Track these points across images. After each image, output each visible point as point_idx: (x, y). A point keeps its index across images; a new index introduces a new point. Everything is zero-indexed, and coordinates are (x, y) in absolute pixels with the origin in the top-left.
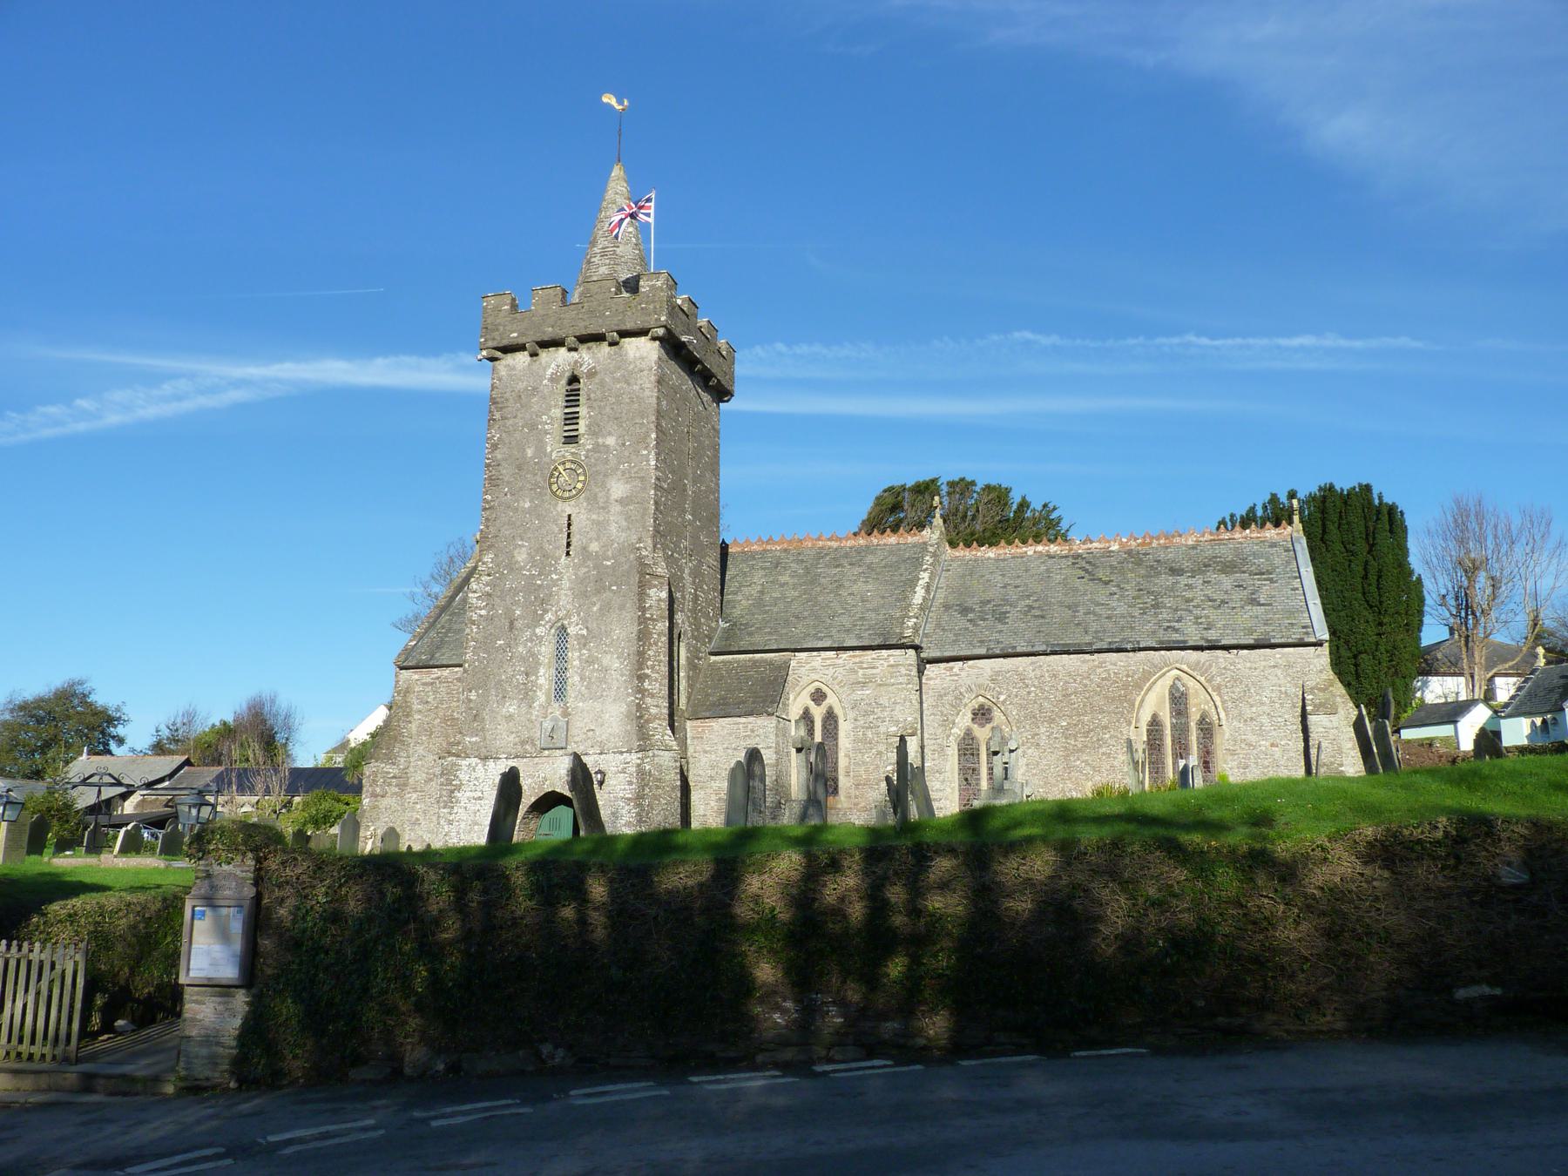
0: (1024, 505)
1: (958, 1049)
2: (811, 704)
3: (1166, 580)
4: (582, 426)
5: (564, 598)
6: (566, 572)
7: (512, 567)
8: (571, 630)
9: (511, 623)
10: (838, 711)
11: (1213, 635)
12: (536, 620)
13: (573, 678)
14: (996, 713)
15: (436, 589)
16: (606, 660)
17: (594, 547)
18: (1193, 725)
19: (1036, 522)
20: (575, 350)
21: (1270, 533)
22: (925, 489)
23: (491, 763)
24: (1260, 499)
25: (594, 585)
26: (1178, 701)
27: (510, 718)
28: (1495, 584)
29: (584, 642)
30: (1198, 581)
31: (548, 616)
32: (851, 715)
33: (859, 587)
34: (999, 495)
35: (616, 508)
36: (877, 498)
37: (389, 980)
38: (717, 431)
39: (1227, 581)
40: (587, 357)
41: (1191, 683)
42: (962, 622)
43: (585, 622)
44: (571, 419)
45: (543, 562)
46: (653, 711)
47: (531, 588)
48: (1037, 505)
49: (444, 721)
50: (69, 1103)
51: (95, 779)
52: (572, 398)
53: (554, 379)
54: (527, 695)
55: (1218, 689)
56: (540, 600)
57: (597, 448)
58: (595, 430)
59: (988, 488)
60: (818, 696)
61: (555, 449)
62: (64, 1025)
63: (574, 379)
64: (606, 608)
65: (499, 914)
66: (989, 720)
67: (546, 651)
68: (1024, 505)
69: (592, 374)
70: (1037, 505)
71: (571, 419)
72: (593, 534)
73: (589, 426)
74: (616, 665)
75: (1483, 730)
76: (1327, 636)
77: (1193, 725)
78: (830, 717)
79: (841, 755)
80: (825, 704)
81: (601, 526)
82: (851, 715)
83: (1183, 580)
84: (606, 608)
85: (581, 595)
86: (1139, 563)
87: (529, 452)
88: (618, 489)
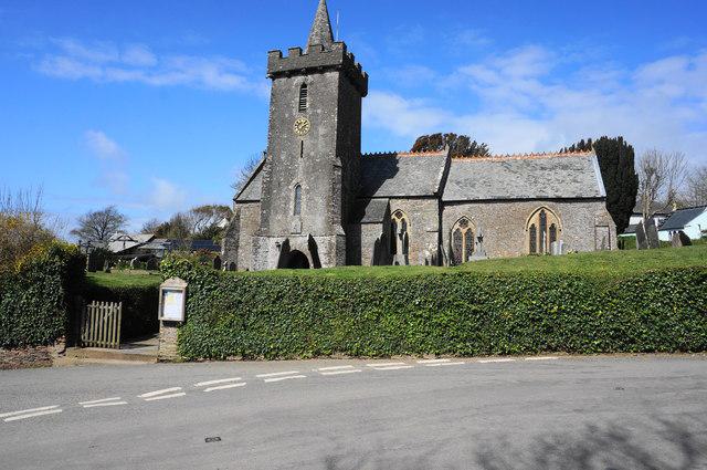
0: (475, 143)
3: (539, 172)
5: (300, 177)
6: (301, 163)
7: (280, 162)
11: (559, 194)
12: (289, 183)
13: (303, 206)
15: (246, 172)
17: (312, 154)
19: (478, 150)
21: (582, 154)
22: (437, 137)
23: (271, 239)
24: (576, 142)
25: (311, 170)
28: (658, 178)
29: (308, 192)
30: (552, 173)
33: (417, 173)
34: (465, 140)
35: (321, 139)
38: (581, 353)
39: (565, 173)
42: (457, 187)
44: (302, 103)
45: (292, 159)
47: (287, 170)
48: (479, 144)
53: (296, 86)
54: (285, 212)
55: (560, 216)
56: (291, 174)
59: (461, 137)
60: (464, 222)
61: (295, 111)
64: (317, 178)
67: (292, 195)
68: (475, 143)
69: (311, 84)
70: (479, 144)
71: (302, 103)
74: (320, 201)
75: (395, 154)
76: (603, 193)
83: (547, 172)
84: (317, 178)
85: (307, 173)
86: (528, 165)
87: (287, 115)
88: (322, 130)
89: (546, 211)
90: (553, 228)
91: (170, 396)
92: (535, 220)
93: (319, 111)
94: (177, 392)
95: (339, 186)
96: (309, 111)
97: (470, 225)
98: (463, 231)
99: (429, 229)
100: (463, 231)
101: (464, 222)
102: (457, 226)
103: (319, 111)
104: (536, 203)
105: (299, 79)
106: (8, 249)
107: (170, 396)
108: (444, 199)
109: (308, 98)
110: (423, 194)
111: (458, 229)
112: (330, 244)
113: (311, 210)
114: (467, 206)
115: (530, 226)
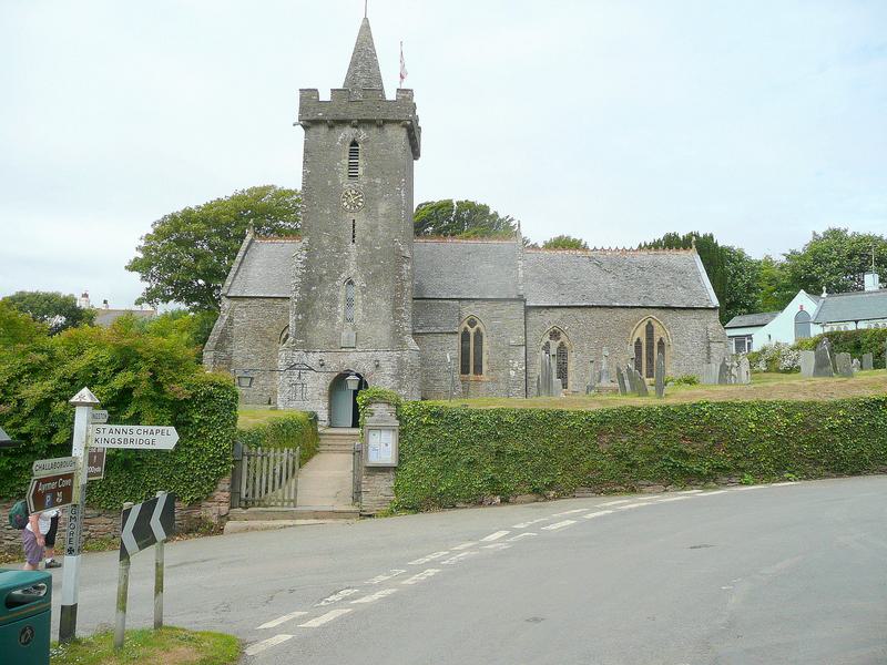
0: (496, 215)
4: (361, 171)
5: (352, 269)
9: (321, 278)
10: (483, 330)
14: (562, 335)
18: (656, 344)
20: (356, 127)
26: (650, 330)
32: (490, 333)
36: (485, 209)
37: (770, 455)
40: (363, 134)
41: (657, 325)
44: (353, 166)
46: (406, 329)
49: (254, 327)
50: (294, 526)
51: (297, 366)
52: (354, 153)
54: (331, 318)
57: (369, 184)
58: (368, 172)
60: (472, 323)
61: (343, 179)
63: (354, 144)
66: (559, 339)
69: (365, 142)
71: (353, 166)
73: (365, 171)
76: (715, 302)
77: (656, 344)
78: (478, 334)
79: (484, 354)
81: (374, 228)
82: (490, 333)
85: (361, 264)
89: (653, 323)
90: (661, 343)
92: (641, 333)
93: (378, 181)
94: (463, 551)
96: (363, 180)
98: (472, 331)
99: (512, 342)
101: (555, 335)
102: (547, 339)
103: (378, 181)
104: (642, 311)
105: (347, 133)
106: (231, 405)
108: (531, 303)
109: (361, 162)
110: (505, 296)
112: (400, 361)
114: (559, 313)
115: (635, 340)
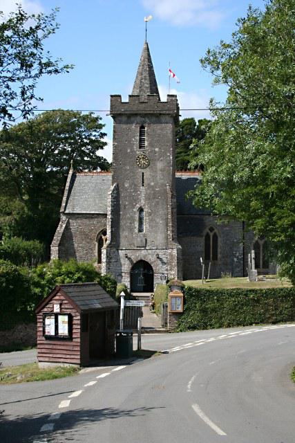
1: (26, 202)
2: (209, 232)
8: (145, 210)
10: (218, 234)
12: (134, 207)
16: (158, 220)
27: (126, 237)
29: (150, 214)
31: (138, 205)
32: (222, 236)
35: (159, 172)
43: (150, 207)
44: (141, 141)
54: (131, 230)
58: (151, 145)
60: (212, 229)
61: (136, 147)
62: (47, 346)
64: (158, 203)
65: (102, 275)
67: (137, 216)
71: (141, 141)
72: (151, 180)
78: (215, 236)
80: (214, 232)
81: (154, 177)
82: (222, 236)
84: (158, 203)
85: (148, 198)
87: (129, 151)
88: (160, 165)
91: (67, 188)
93: (157, 149)
95: (175, 210)
97: (216, 230)
98: (211, 234)
100: (211, 234)
103: (157, 149)
107: (67, 188)
111: (257, 241)
113: (153, 226)
